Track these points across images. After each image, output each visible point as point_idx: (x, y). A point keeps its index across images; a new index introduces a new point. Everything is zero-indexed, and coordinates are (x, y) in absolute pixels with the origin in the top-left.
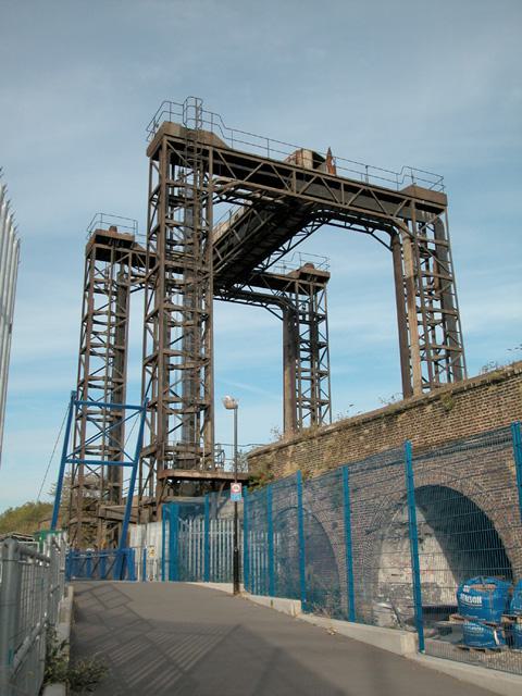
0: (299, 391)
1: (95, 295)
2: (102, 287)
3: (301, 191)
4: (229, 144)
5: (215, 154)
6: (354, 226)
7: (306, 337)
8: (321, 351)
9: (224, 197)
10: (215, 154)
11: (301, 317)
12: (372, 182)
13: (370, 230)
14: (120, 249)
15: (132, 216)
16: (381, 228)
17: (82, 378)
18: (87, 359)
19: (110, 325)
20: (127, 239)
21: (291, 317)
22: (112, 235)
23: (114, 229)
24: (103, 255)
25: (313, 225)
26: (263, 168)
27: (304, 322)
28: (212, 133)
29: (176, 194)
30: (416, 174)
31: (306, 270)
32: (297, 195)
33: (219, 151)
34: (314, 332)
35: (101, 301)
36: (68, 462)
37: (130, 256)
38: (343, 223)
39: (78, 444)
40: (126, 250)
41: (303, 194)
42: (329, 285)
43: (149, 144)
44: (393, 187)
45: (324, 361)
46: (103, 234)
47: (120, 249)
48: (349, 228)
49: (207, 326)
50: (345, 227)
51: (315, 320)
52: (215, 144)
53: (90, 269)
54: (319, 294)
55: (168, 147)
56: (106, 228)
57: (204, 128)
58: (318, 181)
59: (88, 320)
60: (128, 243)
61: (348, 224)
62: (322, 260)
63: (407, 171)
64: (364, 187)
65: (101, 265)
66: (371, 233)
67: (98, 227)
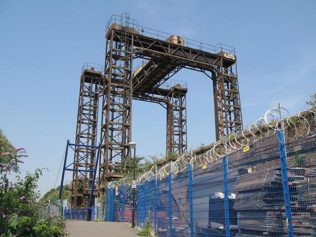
2: (87, 94)
7: (177, 142)
9: (139, 56)
12: (203, 50)
13: (203, 70)
15: (99, 67)
21: (169, 108)
22: (92, 71)
23: (93, 69)
24: (87, 80)
25: (178, 68)
27: (176, 110)
30: (223, 46)
34: (181, 139)
35: (86, 100)
48: (194, 69)
49: (129, 111)
52: (134, 33)
53: (82, 87)
56: (89, 68)
59: (81, 109)
60: (99, 75)
61: (193, 68)
65: (87, 84)
67: (86, 68)
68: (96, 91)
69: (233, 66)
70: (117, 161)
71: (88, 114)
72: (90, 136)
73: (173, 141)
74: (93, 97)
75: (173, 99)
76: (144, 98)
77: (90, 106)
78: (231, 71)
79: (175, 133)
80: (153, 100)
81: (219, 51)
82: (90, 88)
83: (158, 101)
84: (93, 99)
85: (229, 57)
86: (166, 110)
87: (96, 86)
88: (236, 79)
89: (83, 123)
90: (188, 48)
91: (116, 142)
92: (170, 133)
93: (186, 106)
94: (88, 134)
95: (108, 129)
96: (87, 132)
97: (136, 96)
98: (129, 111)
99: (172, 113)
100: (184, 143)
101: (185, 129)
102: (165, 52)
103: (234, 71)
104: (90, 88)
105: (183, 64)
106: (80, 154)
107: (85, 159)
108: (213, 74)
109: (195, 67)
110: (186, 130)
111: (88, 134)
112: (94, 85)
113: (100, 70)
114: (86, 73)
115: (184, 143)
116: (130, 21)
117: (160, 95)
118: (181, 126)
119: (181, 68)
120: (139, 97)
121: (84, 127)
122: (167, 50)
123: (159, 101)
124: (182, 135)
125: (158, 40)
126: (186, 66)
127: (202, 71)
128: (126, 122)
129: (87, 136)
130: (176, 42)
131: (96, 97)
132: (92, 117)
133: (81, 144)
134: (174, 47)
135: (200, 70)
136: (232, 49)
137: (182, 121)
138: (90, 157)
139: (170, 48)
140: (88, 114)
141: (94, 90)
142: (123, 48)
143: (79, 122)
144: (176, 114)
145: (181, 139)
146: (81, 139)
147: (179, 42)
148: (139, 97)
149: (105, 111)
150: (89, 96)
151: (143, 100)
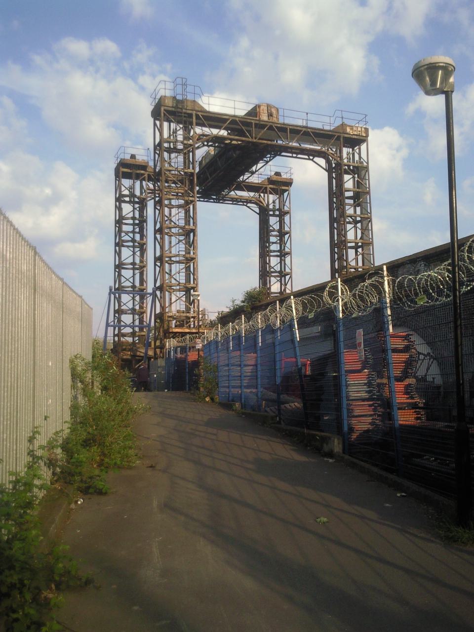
0: (347, 260)
1: (123, 205)
2: (127, 199)
3: (258, 137)
4: (207, 108)
5: (197, 116)
6: (299, 156)
7: (277, 227)
8: (287, 236)
9: (206, 143)
10: (197, 116)
11: (271, 213)
12: (311, 125)
13: (311, 158)
14: (138, 172)
15: (143, 153)
16: (319, 156)
17: (117, 263)
18: (120, 251)
19: (134, 225)
20: (144, 164)
21: (264, 214)
22: (132, 162)
23: (133, 156)
24: (127, 176)
25: (270, 157)
26: (230, 123)
27: (274, 215)
28: (194, 101)
29: (172, 147)
30: (345, 115)
31: (275, 178)
32: (255, 141)
33: (200, 114)
34: (281, 223)
35: (127, 208)
36: (110, 326)
37: (146, 175)
38: (291, 155)
39: (117, 308)
40: (142, 172)
41: (260, 139)
42: (292, 189)
43: (153, 107)
44: (327, 128)
45: (288, 245)
46: (126, 162)
47: (138, 172)
48: (296, 157)
49: (194, 236)
50: (292, 157)
51: (282, 214)
52: (197, 109)
53: (118, 188)
54: (286, 194)
55: (164, 114)
56: (128, 157)
57: (189, 98)
58: (271, 128)
59: (119, 222)
60: (144, 167)
61: (294, 155)
62: (287, 170)
63: (339, 114)
64: (304, 129)
65: (126, 182)
66: (246, 206)
67: (122, 157)
68: (141, 193)
69: (363, 147)
70: (178, 309)
71: (131, 232)
72: (137, 222)
73: (270, 266)
74: (137, 203)
75: (268, 197)
76: (219, 200)
77: (133, 327)
78: (360, 154)
79: (272, 254)
80: (236, 201)
81: (338, 123)
82: (132, 188)
83: (243, 202)
84: (137, 206)
85: (356, 133)
86: (258, 216)
87: (141, 183)
88: (367, 169)
89: (124, 246)
90: (284, 124)
91: (175, 223)
92: (264, 253)
93: (290, 208)
94: (133, 240)
95: (164, 262)
96: (131, 215)
97: (206, 195)
98: (194, 236)
99: (268, 221)
100: (288, 270)
101: (288, 205)
102: (247, 137)
103: (364, 155)
104: (132, 188)
105: (278, 151)
106: (123, 272)
107: (131, 280)
108: (328, 162)
109: (297, 154)
110: (291, 249)
111: (134, 218)
112: (138, 183)
113: (145, 158)
114: (122, 164)
115: (288, 270)
116: (189, 89)
117: (244, 190)
118: (282, 242)
119: (274, 157)
120: (213, 199)
121: (126, 253)
122: (249, 132)
123: (246, 202)
124: (284, 256)
125: (235, 116)
126: (283, 154)
127: (309, 159)
128: (189, 253)
129: (132, 267)
130: (264, 117)
131: (142, 203)
132: (138, 237)
133: (122, 324)
134: (260, 126)
135: (307, 157)
136: (361, 117)
137: (282, 234)
138: (138, 253)
139: (255, 127)
140: (131, 232)
141: (138, 193)
142: (181, 132)
143: (117, 244)
144: (273, 221)
145: (281, 223)
146: (123, 272)
147: (270, 115)
148: (213, 199)
149: (158, 236)
150: (129, 202)
151: (219, 202)
